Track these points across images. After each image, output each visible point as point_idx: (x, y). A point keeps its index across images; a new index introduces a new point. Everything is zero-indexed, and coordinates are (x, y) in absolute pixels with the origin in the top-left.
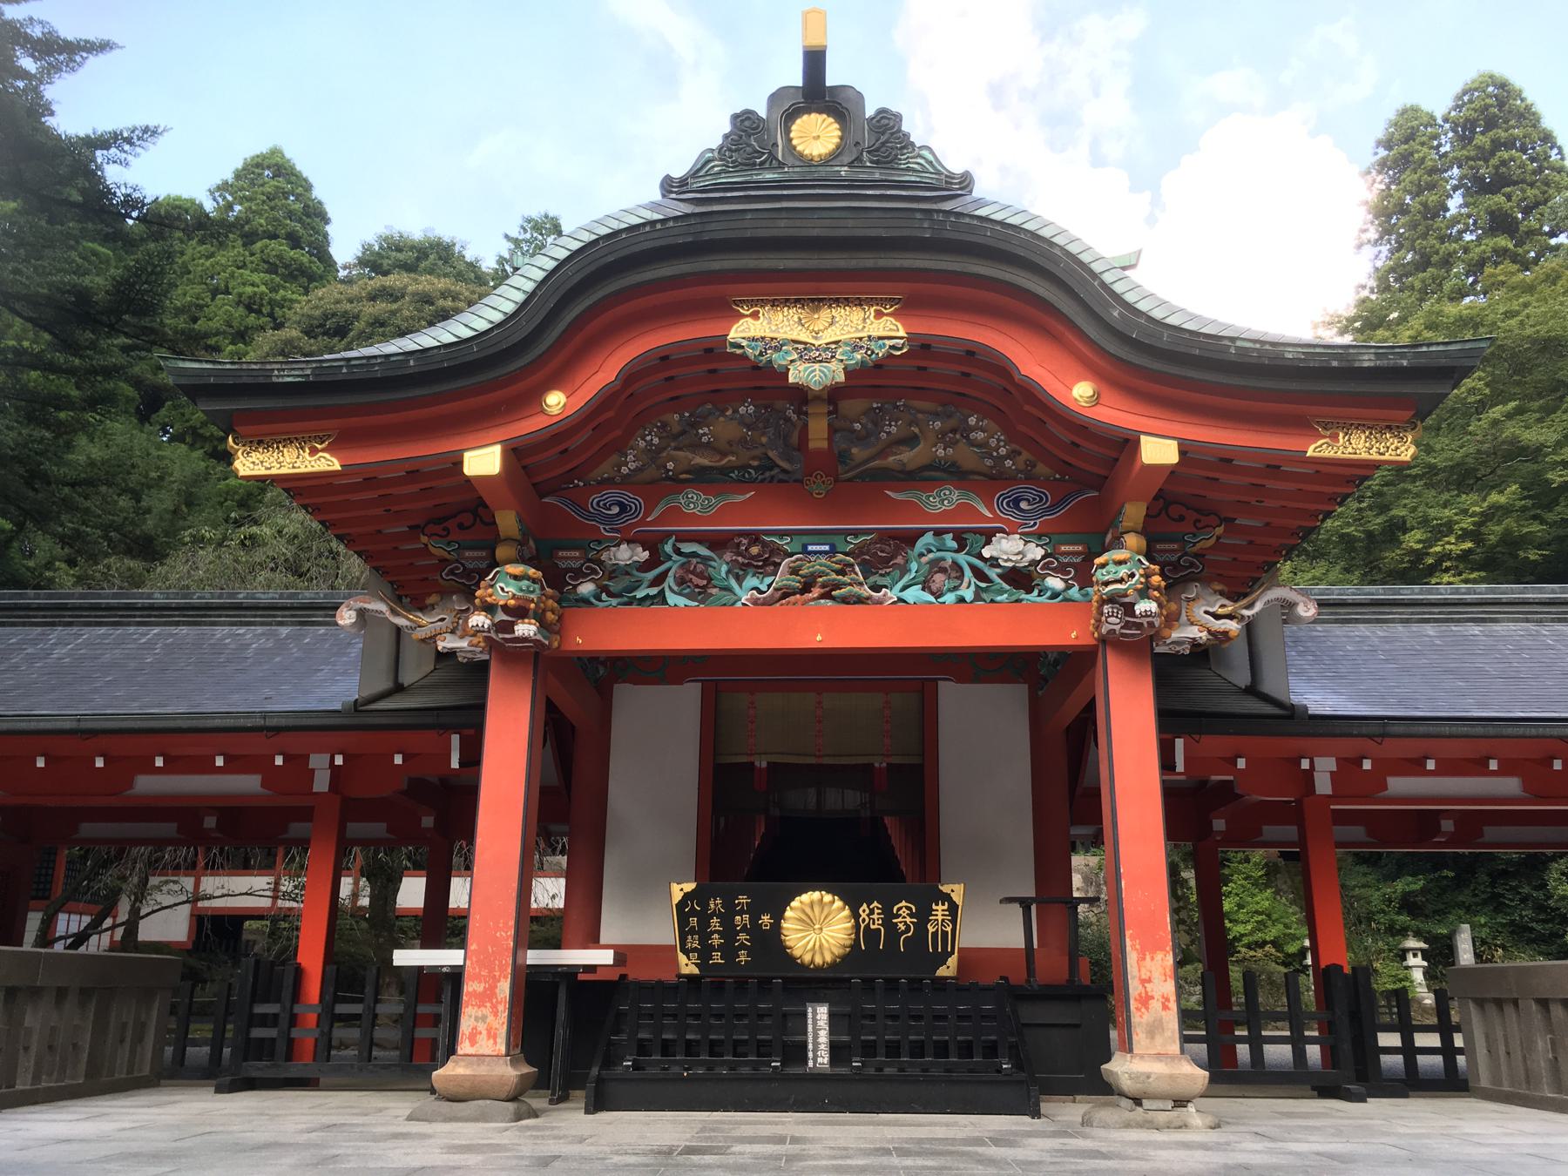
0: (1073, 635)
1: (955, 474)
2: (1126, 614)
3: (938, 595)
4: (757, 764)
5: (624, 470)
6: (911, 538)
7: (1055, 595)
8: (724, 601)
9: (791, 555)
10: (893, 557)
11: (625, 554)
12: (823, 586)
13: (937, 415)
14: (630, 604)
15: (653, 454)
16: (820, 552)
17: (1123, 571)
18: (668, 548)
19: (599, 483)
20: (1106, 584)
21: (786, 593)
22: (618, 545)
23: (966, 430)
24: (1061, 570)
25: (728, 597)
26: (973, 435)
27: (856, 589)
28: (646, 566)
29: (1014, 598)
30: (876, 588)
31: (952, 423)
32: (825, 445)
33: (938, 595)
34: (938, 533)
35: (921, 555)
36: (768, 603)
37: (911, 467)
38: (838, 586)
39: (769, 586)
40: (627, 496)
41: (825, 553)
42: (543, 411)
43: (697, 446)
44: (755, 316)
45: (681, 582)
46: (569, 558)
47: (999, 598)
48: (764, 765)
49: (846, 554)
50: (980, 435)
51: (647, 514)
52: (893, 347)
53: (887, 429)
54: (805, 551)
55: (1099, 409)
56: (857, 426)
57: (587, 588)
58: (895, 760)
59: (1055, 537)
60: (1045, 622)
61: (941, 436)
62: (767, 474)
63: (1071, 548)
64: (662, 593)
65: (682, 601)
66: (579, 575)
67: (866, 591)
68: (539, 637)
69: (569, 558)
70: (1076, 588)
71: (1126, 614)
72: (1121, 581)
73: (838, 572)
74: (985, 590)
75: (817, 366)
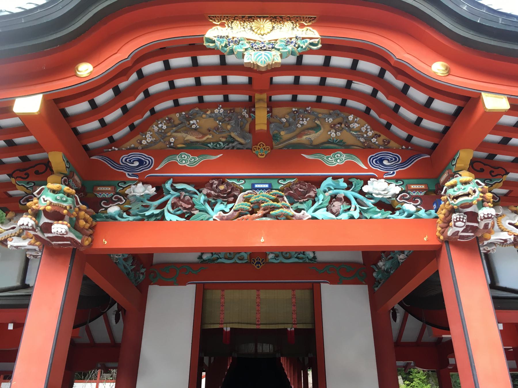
0: (426, 239)
1: (345, 147)
2: (469, 220)
3: (337, 214)
4: (225, 329)
5: (144, 142)
6: (317, 182)
7: (410, 215)
8: (201, 218)
9: (245, 191)
10: (308, 192)
11: (140, 190)
12: (264, 210)
13: (330, 115)
14: (143, 220)
15: (163, 135)
16: (263, 189)
17: (469, 188)
18: (168, 186)
19: (127, 149)
20: (457, 197)
21: (241, 213)
22: (136, 184)
23: (348, 124)
24: (412, 199)
25: (204, 216)
26: (351, 126)
27: (285, 210)
28: (153, 198)
29: (384, 216)
30: (298, 210)
31: (339, 120)
32: (265, 128)
33: (337, 214)
34: (335, 178)
35: (325, 192)
36: (228, 219)
37: (315, 143)
38: (274, 208)
39: (231, 209)
40: (144, 156)
41: (266, 189)
42: (76, 75)
43: (189, 130)
44: (223, 25)
45: (174, 206)
46: (104, 191)
47: (375, 216)
48: (229, 329)
49: (279, 190)
50: (356, 125)
51: (156, 166)
52: (311, 44)
53: (301, 122)
54: (253, 188)
55: (450, 77)
56: (284, 120)
57: (113, 210)
58: (299, 326)
59: (406, 181)
60: (409, 226)
61: (333, 126)
62: (231, 145)
63: (417, 187)
64: (162, 213)
65: (175, 218)
66: (110, 202)
67: (291, 212)
68: (71, 235)
69: (104, 191)
70: (423, 210)
71: (469, 220)
72: (468, 195)
73: (274, 201)
74: (366, 211)
75: (263, 52)
